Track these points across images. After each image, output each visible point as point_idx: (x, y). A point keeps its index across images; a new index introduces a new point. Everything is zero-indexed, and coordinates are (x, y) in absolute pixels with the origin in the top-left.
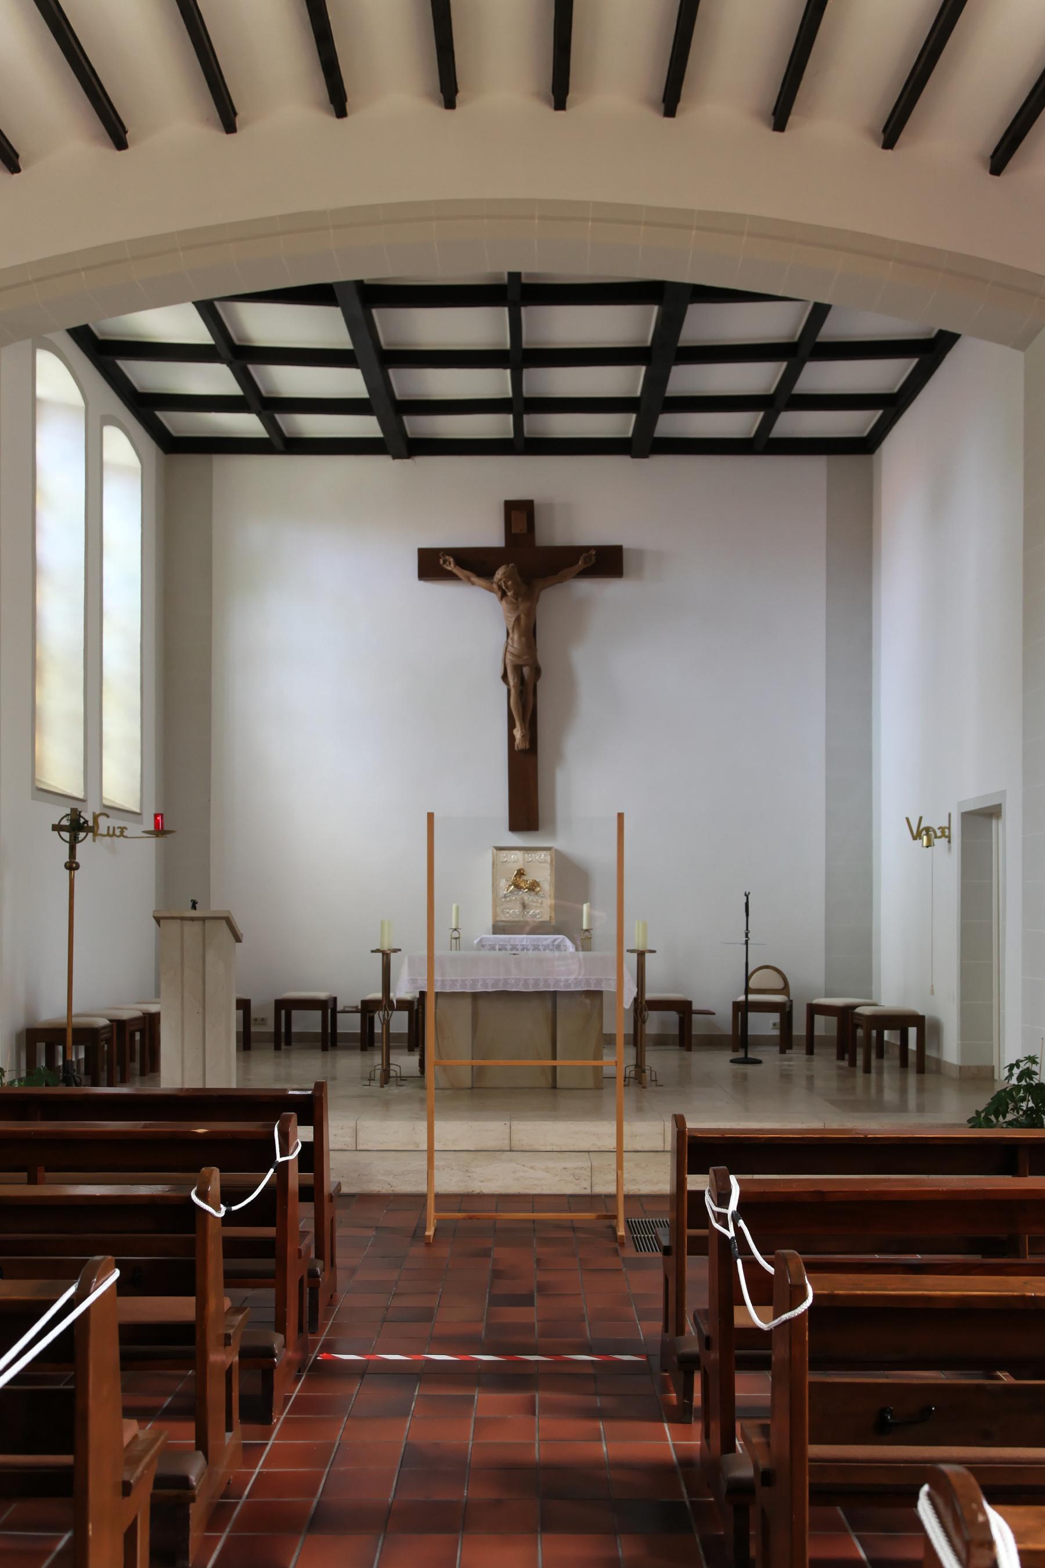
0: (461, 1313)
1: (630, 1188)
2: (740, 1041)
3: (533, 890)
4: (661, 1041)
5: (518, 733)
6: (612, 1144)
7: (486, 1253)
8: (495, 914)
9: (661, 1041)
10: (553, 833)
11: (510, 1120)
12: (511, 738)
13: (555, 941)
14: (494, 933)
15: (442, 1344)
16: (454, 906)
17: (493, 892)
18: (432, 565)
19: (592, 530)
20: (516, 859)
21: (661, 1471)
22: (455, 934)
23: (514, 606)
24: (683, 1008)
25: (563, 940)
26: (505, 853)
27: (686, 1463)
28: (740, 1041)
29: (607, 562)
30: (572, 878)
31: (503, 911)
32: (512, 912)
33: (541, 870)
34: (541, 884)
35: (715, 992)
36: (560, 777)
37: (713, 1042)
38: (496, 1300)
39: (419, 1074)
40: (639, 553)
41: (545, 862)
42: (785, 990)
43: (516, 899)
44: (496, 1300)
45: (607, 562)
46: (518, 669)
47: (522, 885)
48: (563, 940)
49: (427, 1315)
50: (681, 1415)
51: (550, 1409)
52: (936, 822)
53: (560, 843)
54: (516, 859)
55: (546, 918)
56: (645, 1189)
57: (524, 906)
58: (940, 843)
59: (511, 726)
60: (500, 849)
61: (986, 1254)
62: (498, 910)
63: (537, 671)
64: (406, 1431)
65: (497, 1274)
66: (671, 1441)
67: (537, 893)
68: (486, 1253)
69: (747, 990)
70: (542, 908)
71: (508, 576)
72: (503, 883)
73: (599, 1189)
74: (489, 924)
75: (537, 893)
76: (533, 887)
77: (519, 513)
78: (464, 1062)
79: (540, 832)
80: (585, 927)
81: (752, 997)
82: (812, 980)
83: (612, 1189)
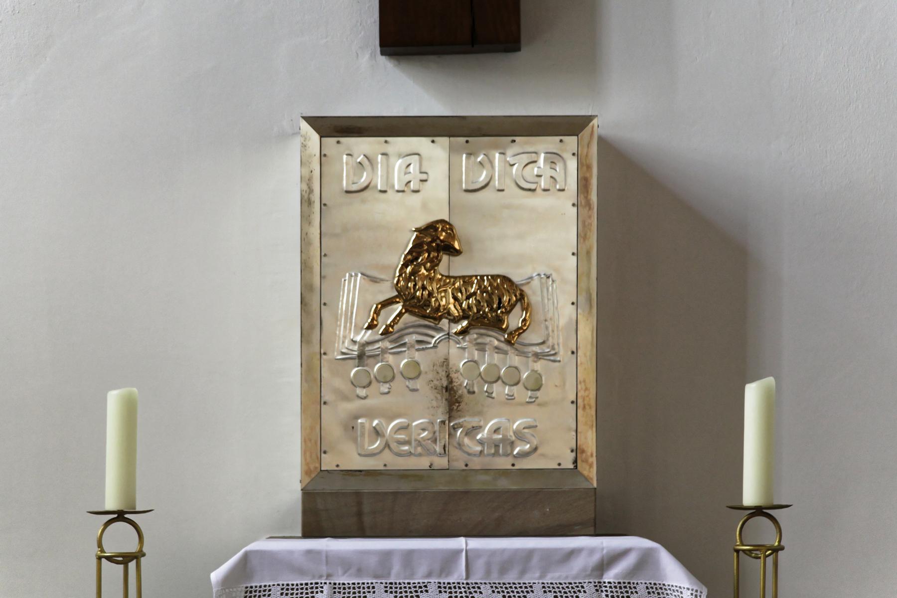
3: (496, 324)
8: (315, 443)
10: (585, 59)
13: (603, 566)
14: (308, 534)
16: (114, 399)
17: (305, 338)
20: (413, 182)
22: (121, 539)
25: (646, 561)
26: (362, 145)
31: (350, 427)
32: (396, 430)
33: (535, 226)
34: (533, 294)
39: (572, 466)
41: (554, 188)
43: (414, 372)
47: (447, 301)
48: (646, 561)
53: (619, 109)
54: (413, 182)
55: (556, 454)
57: (452, 398)
60: (334, 128)
61: (312, 328)
62: (332, 419)
67: (513, 339)
70: (541, 412)
72: (354, 297)
74: (288, 489)
75: (513, 339)
76: (495, 307)
79: (525, 54)
80: (750, 496)
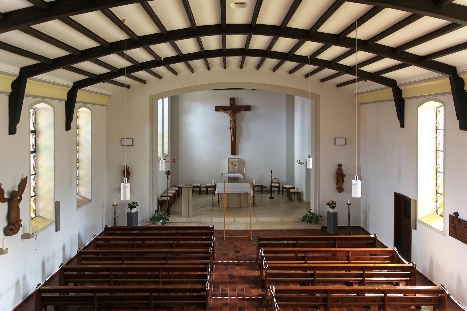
0: (232, 254)
1: (253, 229)
2: (271, 191)
4: (257, 191)
5: (232, 138)
6: (250, 221)
7: (233, 243)
9: (257, 191)
10: (238, 155)
11: (234, 217)
12: (231, 139)
15: (230, 259)
18: (217, 109)
19: (245, 102)
21: (256, 277)
23: (232, 117)
24: (261, 187)
27: (259, 276)
28: (271, 191)
29: (248, 108)
30: (242, 163)
35: (267, 183)
36: (240, 145)
37: (266, 191)
38: (236, 252)
40: (254, 106)
42: (279, 183)
44: (236, 252)
45: (248, 108)
46: (233, 128)
49: (226, 254)
50: (258, 270)
51: (244, 269)
52: (302, 161)
56: (255, 229)
58: (303, 164)
59: (231, 137)
63: (236, 128)
64: (228, 272)
65: (235, 247)
66: (257, 273)
68: (233, 243)
69: (272, 183)
71: (231, 112)
73: (248, 229)
77: (233, 100)
78: (225, 205)
81: (273, 184)
82: (283, 178)
83: (250, 229)
